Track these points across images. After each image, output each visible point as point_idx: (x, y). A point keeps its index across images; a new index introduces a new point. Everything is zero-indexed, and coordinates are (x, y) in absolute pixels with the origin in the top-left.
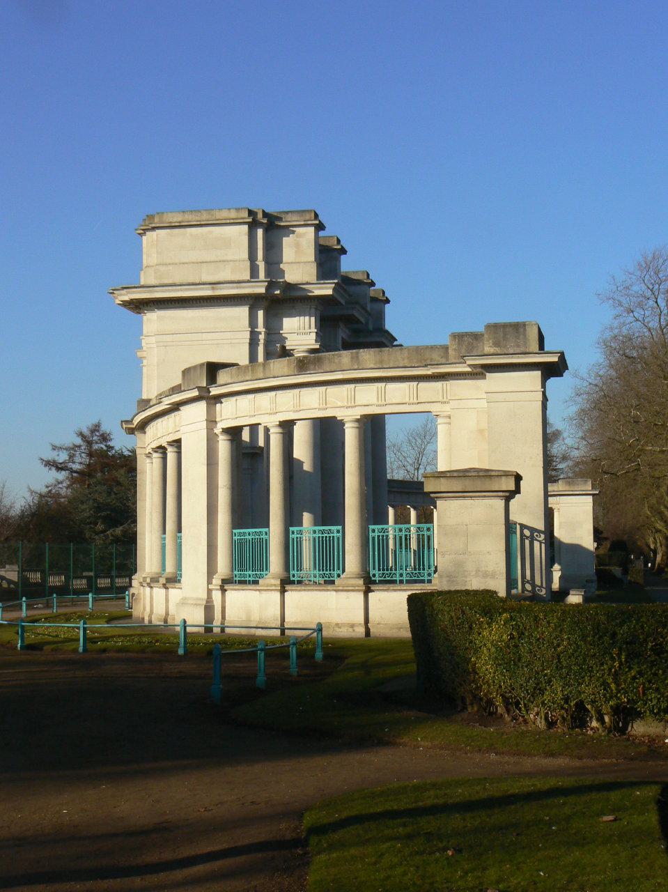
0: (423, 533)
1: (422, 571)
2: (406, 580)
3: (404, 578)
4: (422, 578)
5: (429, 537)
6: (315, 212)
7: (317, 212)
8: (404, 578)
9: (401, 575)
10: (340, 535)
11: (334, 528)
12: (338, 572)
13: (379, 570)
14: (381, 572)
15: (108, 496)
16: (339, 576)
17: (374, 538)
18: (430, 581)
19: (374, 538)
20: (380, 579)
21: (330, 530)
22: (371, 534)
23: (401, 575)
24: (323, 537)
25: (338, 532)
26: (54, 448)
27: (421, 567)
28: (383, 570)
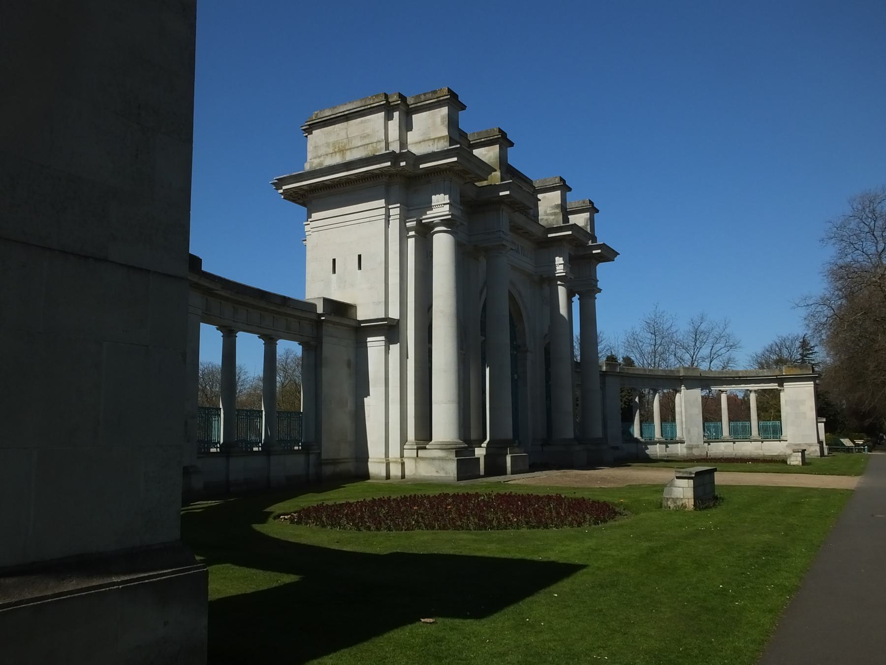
10: (780, 424)
22: (731, 425)
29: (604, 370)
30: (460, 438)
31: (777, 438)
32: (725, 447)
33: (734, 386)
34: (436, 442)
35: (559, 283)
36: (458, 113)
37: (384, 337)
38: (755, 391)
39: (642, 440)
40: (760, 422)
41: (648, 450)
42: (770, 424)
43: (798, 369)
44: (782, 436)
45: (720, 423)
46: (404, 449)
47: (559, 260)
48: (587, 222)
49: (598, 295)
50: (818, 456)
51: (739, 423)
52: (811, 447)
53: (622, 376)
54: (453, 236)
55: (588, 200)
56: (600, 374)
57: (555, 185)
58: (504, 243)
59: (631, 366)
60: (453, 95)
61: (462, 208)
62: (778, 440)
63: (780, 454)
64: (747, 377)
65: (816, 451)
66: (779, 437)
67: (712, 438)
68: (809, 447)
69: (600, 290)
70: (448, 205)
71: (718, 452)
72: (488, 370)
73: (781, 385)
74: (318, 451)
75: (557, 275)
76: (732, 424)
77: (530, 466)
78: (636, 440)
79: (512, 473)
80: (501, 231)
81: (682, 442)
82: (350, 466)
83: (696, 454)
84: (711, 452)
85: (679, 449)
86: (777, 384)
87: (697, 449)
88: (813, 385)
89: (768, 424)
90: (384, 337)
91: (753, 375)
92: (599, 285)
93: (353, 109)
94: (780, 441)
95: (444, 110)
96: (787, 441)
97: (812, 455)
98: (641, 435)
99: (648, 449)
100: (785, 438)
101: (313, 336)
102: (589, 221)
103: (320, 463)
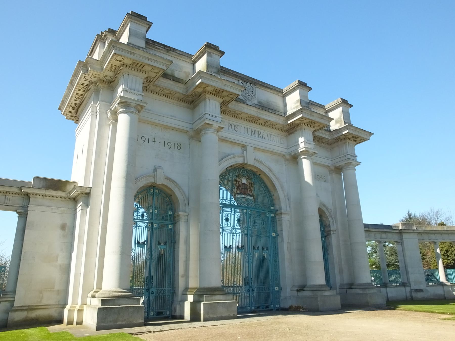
29: (401, 229)
30: (120, 287)
34: (105, 291)
35: (303, 157)
36: (308, 93)
39: (448, 284)
46: (88, 297)
47: (301, 140)
48: (341, 114)
49: (357, 168)
53: (419, 233)
54: (309, 160)
55: (340, 98)
56: (365, 230)
57: (294, 87)
58: (350, 161)
59: (424, 225)
60: (344, 102)
61: (315, 144)
69: (358, 164)
70: (304, 143)
74: (12, 299)
75: (300, 151)
77: (342, 305)
78: (442, 284)
79: (205, 320)
80: (348, 154)
82: (53, 313)
92: (358, 159)
93: (162, 73)
95: (340, 109)
98: (448, 280)
101: (23, 206)
102: (342, 113)
103: (12, 308)
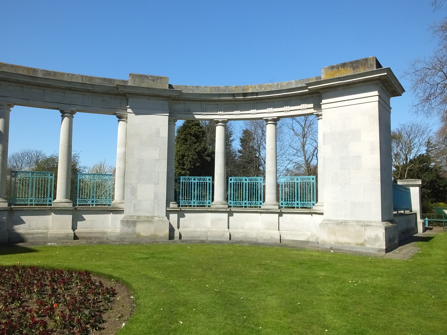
0: (206, 181)
1: (205, 201)
2: (197, 205)
3: (196, 204)
4: (257, 205)
5: (264, 186)
6: (376, 58)
7: (377, 58)
8: (247, 205)
9: (298, 204)
10: (211, 182)
11: (208, 178)
12: (313, 202)
13: (233, 200)
14: (286, 202)
15: (205, 147)
16: (313, 204)
17: (231, 184)
18: (209, 206)
19: (231, 184)
20: (234, 205)
21: (204, 179)
22: (230, 182)
23: (298, 204)
24: (303, 182)
25: (313, 179)
26: (321, 118)
27: (252, 199)
28: (287, 201)
31: (294, 208)
32: (213, 222)
33: (238, 112)
37: (377, 92)
38: (223, 122)
40: (230, 178)
41: (22, 226)
42: (299, 181)
43: (349, 68)
44: (317, 204)
45: (314, 177)
50: (380, 250)
51: (244, 178)
52: (368, 229)
62: (307, 211)
63: (310, 240)
64: (257, 94)
65: (377, 239)
66: (208, 204)
67: (192, 204)
68: (363, 228)
71: (198, 229)
72: (193, 113)
73: (318, 106)
76: (232, 181)
81: (117, 211)
83: (143, 234)
84: (185, 230)
85: (110, 223)
86: (311, 105)
87: (147, 225)
88: (377, 98)
89: (193, 181)
90: (377, 92)
91: (269, 89)
94: (311, 214)
96: (322, 214)
97: (368, 246)
99: (23, 222)
100: (316, 208)
